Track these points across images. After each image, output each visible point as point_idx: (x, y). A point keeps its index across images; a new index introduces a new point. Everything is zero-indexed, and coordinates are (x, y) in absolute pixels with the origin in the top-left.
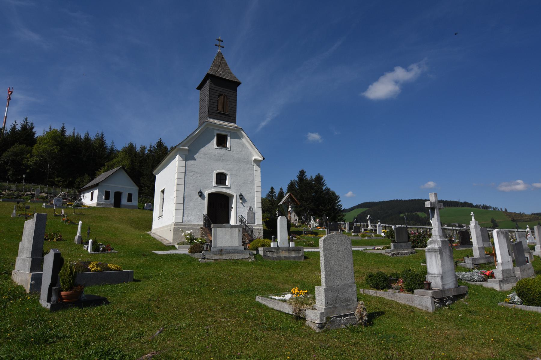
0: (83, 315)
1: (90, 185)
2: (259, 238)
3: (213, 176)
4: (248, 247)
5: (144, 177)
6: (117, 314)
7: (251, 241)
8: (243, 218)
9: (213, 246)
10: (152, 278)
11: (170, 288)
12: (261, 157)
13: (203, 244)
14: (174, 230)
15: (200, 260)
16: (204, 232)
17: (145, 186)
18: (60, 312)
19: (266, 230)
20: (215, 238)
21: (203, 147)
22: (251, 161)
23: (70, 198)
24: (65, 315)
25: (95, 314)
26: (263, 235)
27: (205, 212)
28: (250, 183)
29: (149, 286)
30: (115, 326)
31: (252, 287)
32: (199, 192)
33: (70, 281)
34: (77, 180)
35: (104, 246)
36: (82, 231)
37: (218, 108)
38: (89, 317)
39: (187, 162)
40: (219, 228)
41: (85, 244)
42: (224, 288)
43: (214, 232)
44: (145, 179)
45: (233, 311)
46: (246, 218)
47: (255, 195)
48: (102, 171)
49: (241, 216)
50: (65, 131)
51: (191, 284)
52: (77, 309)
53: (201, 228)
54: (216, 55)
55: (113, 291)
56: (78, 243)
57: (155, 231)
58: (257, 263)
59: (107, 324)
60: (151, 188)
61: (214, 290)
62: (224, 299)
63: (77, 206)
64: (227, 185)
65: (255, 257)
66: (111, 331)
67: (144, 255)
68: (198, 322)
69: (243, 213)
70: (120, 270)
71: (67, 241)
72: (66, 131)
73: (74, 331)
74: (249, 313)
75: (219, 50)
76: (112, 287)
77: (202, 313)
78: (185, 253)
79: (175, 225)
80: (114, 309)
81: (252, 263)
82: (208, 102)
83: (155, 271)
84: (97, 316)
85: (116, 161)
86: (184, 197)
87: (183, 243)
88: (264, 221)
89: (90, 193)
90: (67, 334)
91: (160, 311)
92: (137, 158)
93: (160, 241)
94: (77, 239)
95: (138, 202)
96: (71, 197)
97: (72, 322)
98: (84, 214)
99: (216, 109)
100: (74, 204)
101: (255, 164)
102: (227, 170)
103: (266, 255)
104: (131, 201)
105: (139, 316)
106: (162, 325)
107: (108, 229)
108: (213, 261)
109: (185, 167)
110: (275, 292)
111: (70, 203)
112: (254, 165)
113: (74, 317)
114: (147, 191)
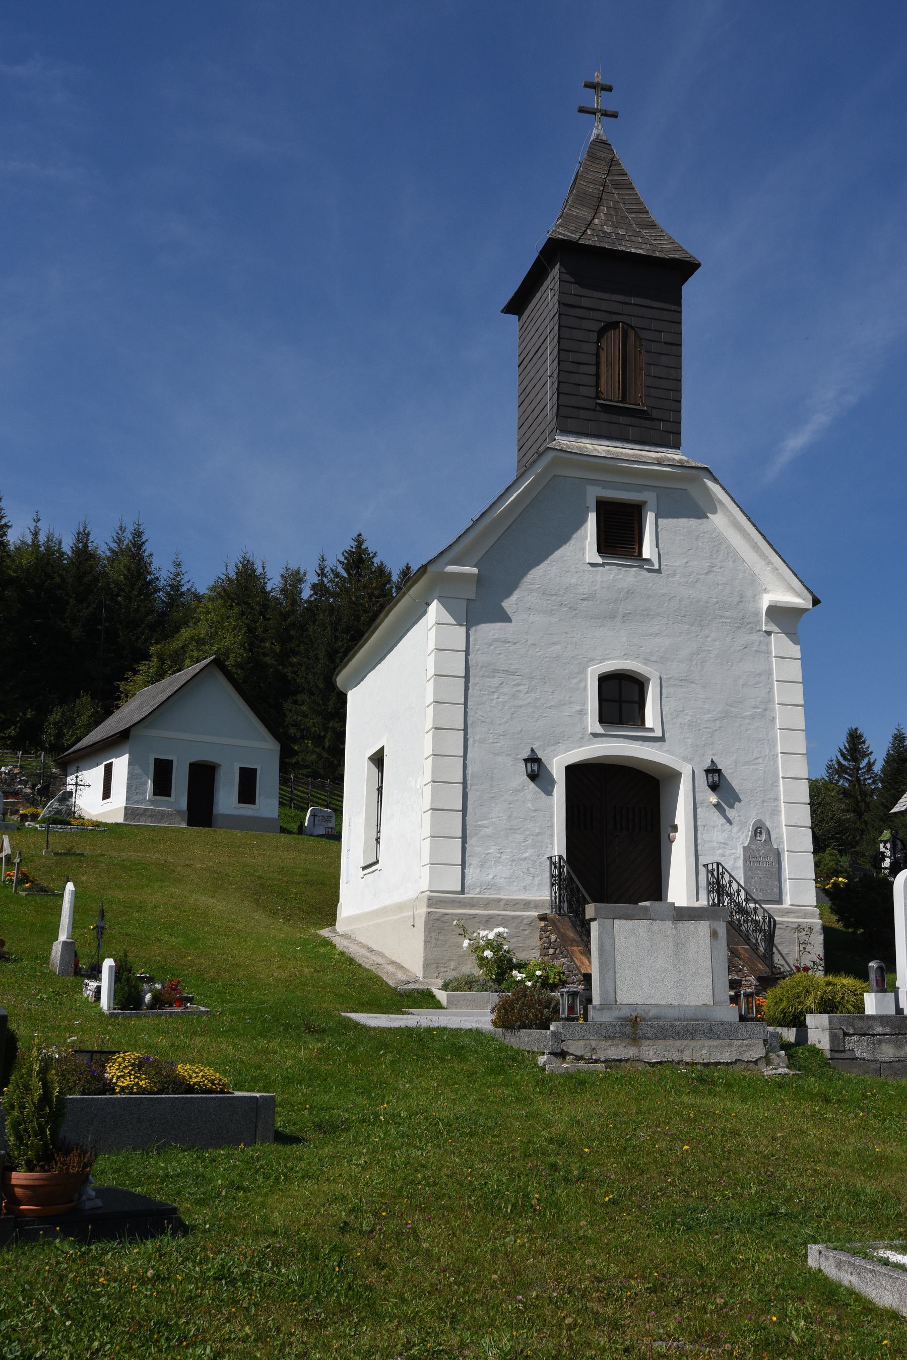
0: (92, 1273)
1: (98, 738)
2: (806, 969)
3: (586, 687)
4: (758, 1012)
5: (300, 697)
6: (217, 1279)
7: (768, 980)
8: (727, 876)
9: (596, 1001)
10: (347, 1130)
11: (424, 1178)
12: (799, 595)
13: (554, 987)
14: (426, 923)
15: (542, 1060)
16: (553, 937)
17: (303, 737)
18: (8, 1252)
19: (831, 928)
20: (607, 964)
21: (538, 564)
22: (757, 614)
23: (29, 790)
24: (27, 1268)
25: (136, 1272)
26: (822, 956)
27: (558, 847)
28: (752, 717)
29: (340, 1164)
30: (215, 1331)
31: (787, 1200)
32: (526, 761)
33: (42, 1132)
34: (52, 719)
35: (158, 986)
36: (75, 925)
37: (597, 385)
38: (116, 1285)
39: (471, 632)
40: (623, 922)
41: (89, 977)
42: (655, 1197)
43: (600, 938)
44: (304, 708)
45: (704, 1308)
46: (740, 876)
47: (777, 769)
48: (139, 678)
49: (718, 864)
50: (6, 526)
51: (512, 1170)
52: (66, 1247)
53: (543, 918)
54: (582, 156)
55: (198, 1177)
56: (63, 972)
57: (351, 928)
58: (802, 1088)
59: (183, 1320)
60: (327, 744)
61: (614, 1202)
62: (660, 1246)
63: (55, 822)
64: (647, 726)
65: (790, 1056)
66: (199, 1351)
67: (311, 1030)
68: (551, 1346)
69: (727, 853)
70: (222, 1092)
71: (25, 963)
72: (8, 527)
73: (60, 1337)
74: (779, 1323)
75: (597, 130)
76: (196, 1162)
77: (566, 1303)
78: (479, 1026)
79: (432, 902)
80: (206, 1259)
81: (780, 1084)
82: (556, 362)
83: (358, 1100)
84: (143, 1281)
85: (192, 638)
86: (464, 783)
87: (469, 984)
88: (826, 891)
89: (100, 770)
90: (36, 1349)
91: (388, 1278)
92: (269, 619)
93: (373, 968)
94: (59, 953)
95: (280, 803)
96: (33, 788)
97: (52, 1301)
98: (82, 855)
99: (591, 392)
100: (43, 813)
101: (773, 628)
102: (647, 661)
103: (844, 1051)
104: (253, 802)
105: (305, 1296)
106: (399, 1346)
107: (171, 916)
108: (600, 1067)
109: (467, 652)
110: (901, 1234)
111: (30, 810)
112: (769, 633)
113: (61, 1280)
114: (314, 757)
